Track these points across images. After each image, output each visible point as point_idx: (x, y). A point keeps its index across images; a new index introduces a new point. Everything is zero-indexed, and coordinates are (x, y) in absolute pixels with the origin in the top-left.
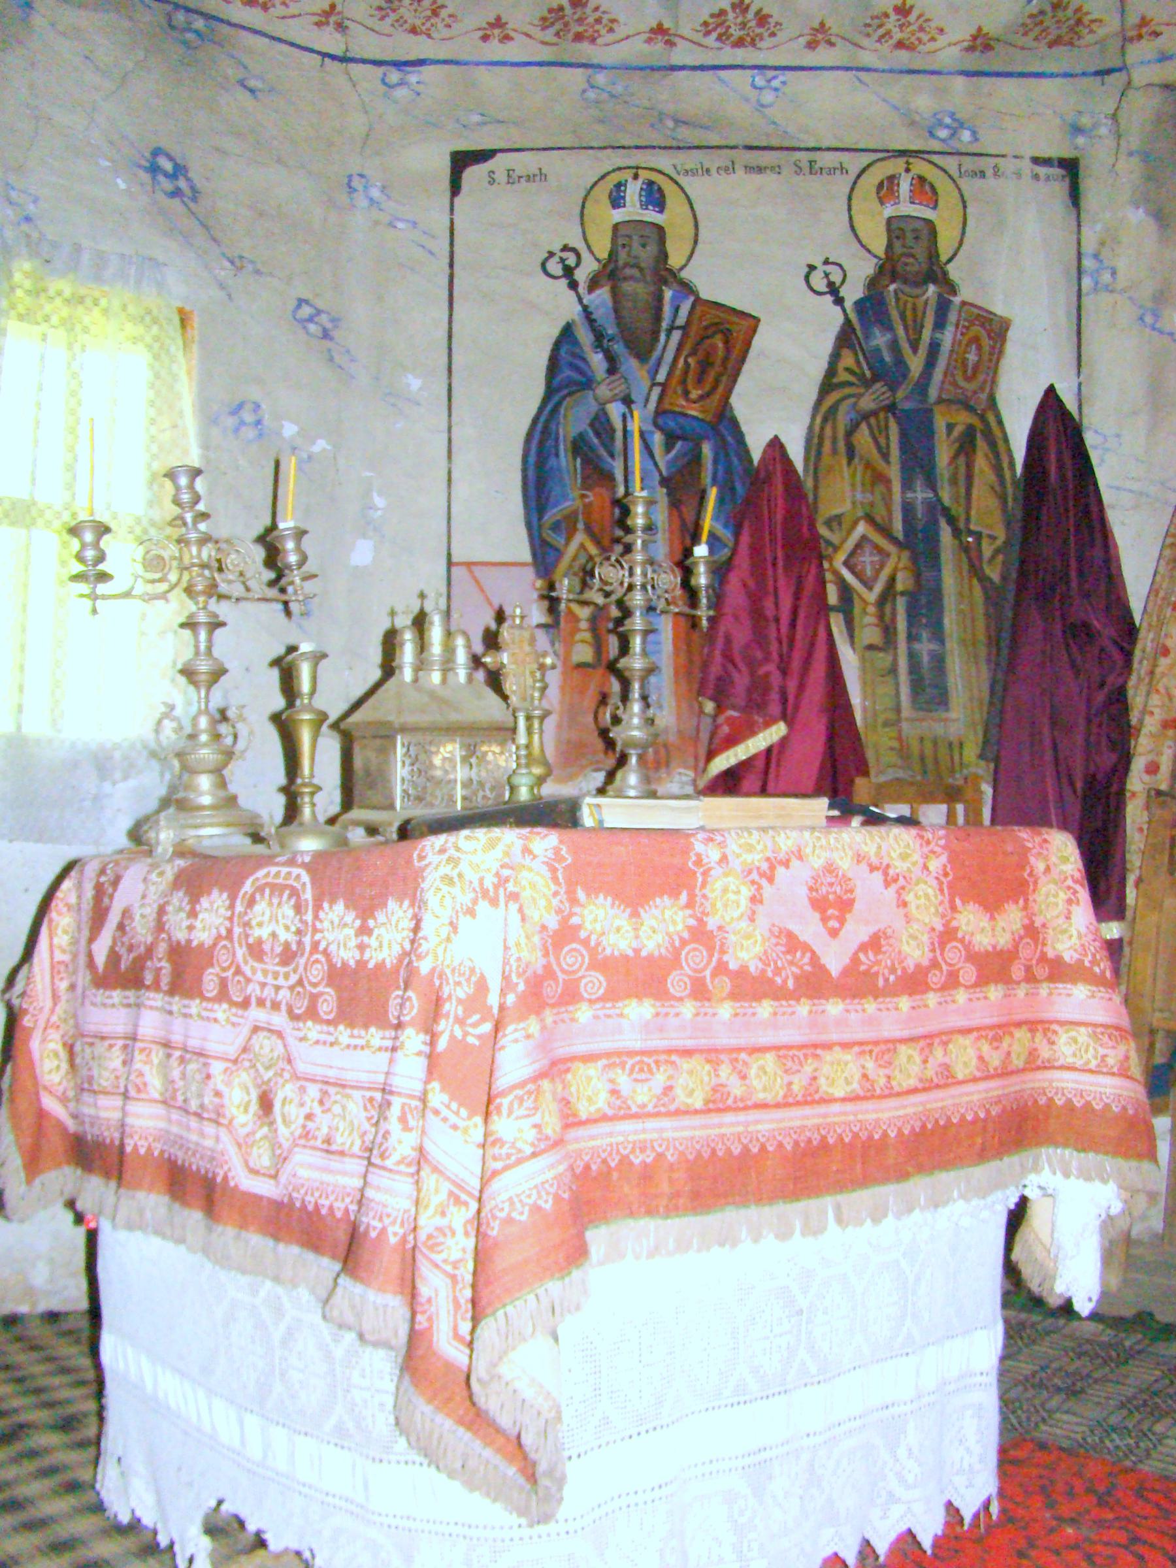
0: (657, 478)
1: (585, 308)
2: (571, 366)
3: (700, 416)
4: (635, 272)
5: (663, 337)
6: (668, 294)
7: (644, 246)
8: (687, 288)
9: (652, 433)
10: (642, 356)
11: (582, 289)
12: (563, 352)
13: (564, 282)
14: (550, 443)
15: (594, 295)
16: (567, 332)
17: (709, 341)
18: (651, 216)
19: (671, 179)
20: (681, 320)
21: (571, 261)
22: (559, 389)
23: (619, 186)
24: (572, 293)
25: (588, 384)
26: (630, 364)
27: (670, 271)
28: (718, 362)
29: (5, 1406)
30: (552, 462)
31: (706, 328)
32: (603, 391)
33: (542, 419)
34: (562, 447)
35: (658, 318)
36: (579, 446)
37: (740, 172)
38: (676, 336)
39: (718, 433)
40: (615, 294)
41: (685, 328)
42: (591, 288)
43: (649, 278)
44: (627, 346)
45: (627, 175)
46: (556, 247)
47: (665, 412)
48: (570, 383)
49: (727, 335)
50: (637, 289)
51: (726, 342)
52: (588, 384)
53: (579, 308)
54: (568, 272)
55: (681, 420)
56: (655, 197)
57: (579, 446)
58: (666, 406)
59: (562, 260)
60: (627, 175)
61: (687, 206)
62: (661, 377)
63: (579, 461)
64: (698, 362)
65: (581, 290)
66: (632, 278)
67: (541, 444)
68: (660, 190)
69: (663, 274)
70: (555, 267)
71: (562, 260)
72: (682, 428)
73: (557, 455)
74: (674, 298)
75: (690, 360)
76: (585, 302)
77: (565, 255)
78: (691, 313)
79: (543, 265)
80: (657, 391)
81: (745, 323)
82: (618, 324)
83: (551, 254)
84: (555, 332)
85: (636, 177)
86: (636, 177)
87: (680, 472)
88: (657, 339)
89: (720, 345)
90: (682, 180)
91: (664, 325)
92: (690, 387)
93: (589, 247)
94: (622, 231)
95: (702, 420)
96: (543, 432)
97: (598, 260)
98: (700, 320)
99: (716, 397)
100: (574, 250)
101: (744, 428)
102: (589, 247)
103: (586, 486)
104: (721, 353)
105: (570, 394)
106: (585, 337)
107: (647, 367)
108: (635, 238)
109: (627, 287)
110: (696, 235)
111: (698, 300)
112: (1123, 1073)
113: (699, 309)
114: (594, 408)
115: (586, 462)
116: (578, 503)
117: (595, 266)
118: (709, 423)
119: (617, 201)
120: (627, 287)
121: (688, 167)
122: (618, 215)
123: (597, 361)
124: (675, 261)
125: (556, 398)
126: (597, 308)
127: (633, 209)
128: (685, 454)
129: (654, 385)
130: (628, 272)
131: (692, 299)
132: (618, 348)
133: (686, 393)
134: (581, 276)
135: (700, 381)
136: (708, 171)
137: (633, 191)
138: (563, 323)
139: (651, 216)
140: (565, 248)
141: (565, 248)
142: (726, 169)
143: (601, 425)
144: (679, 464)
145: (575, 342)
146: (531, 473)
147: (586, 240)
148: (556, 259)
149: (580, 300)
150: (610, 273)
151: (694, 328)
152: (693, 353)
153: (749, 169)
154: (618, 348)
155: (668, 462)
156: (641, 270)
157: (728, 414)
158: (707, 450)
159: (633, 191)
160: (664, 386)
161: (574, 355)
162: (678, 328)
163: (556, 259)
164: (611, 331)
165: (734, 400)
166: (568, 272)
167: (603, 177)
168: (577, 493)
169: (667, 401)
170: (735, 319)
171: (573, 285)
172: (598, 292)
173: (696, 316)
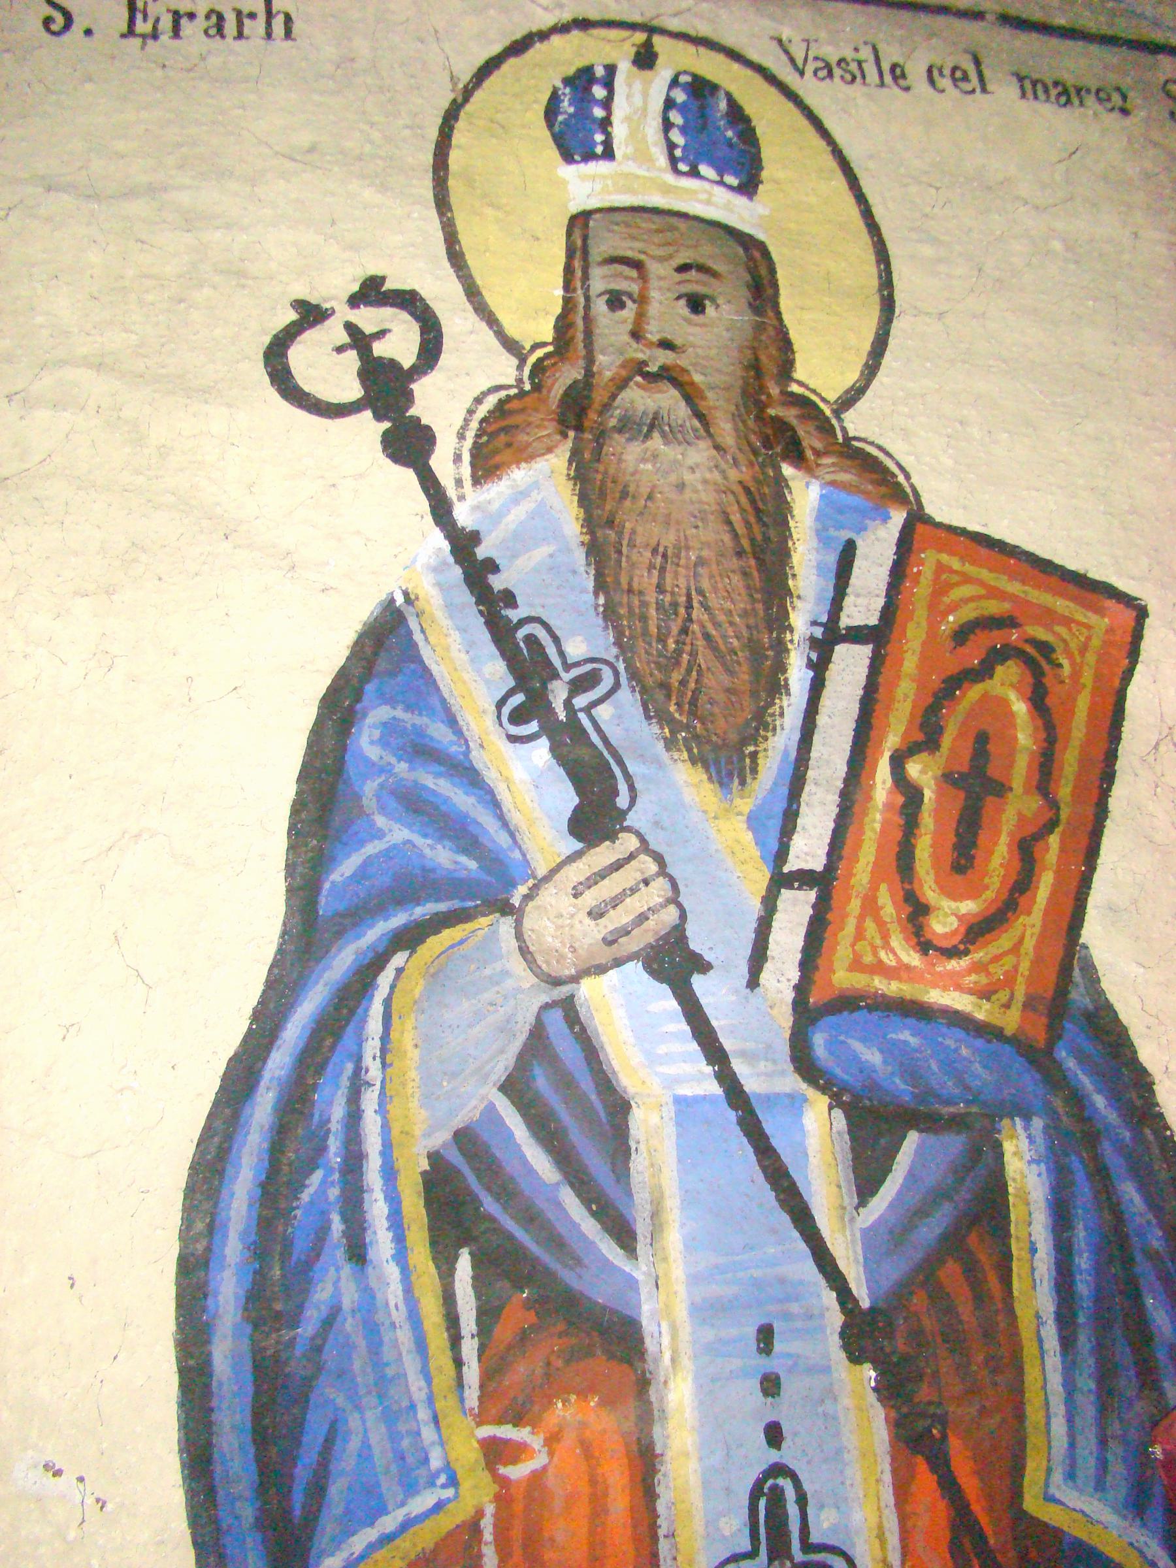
0: (836, 1319)
1: (463, 545)
2: (415, 805)
3: (982, 1012)
4: (668, 400)
5: (798, 675)
6: (806, 496)
7: (696, 304)
8: (877, 478)
9: (796, 1103)
10: (728, 762)
11: (445, 462)
12: (367, 741)
13: (368, 429)
14: (320, 1185)
15: (497, 491)
16: (386, 642)
17: (974, 692)
18: (709, 198)
19: (771, 79)
20: (861, 609)
21: (400, 343)
22: (356, 916)
23: (581, 81)
24: (408, 476)
25: (494, 890)
26: (671, 790)
27: (806, 406)
28: (1020, 772)
29: (5, 472)
30: (334, 1284)
31: (962, 635)
32: (559, 919)
33: (279, 1062)
34: (377, 1209)
35: (773, 587)
36: (458, 1200)
37: (1005, 92)
38: (851, 665)
39: (1054, 1078)
40: (596, 492)
41: (879, 636)
42: (486, 465)
43: (725, 430)
44: (653, 712)
45: (616, 50)
46: (334, 286)
47: (847, 1002)
48: (409, 885)
49: (1038, 661)
50: (682, 473)
51: (1038, 700)
52: (494, 890)
53: (438, 541)
54: (386, 389)
55: (906, 1035)
56: (711, 129)
57: (458, 1200)
58: (843, 978)
59: (359, 340)
60: (616, 50)
61: (839, 183)
62: (809, 849)
63: (464, 1265)
64: (948, 778)
65: (441, 463)
66: (655, 423)
67: (276, 1190)
68: (736, 114)
69: (781, 426)
70: (326, 367)
71: (359, 340)
72: (912, 1073)
73: (358, 1253)
74: (826, 516)
75: (913, 769)
76: (463, 516)
77: (368, 318)
78: (899, 571)
79: (276, 356)
80: (796, 908)
81: (1101, 623)
82: (610, 614)
83: (311, 315)
84: (333, 651)
85: (645, 59)
86: (645, 59)
87: (925, 1275)
88: (776, 687)
89: (1020, 707)
90: (811, 90)
91: (802, 620)
92: (930, 893)
93: (473, 293)
94: (605, 243)
95: (980, 1030)
96: (281, 1132)
97: (511, 345)
98: (937, 611)
99: (1030, 924)
100: (408, 301)
101: (1148, 1054)
102: (473, 293)
103: (505, 1401)
104: (1025, 738)
105: (409, 938)
106: (468, 672)
107: (745, 805)
108: (655, 269)
109: (631, 457)
110: (886, 283)
111: (917, 518)
112: (708, 449)
113: (927, 561)
114: (526, 999)
115: (502, 1265)
116: (476, 1494)
117: (505, 371)
118: (1020, 1044)
119: (577, 125)
120: (631, 457)
121: (832, 54)
122: (585, 186)
123: (529, 784)
124: (821, 369)
125: (342, 961)
126: (521, 541)
127: (638, 167)
128: (939, 1195)
129: (781, 881)
130: (639, 399)
131: (898, 517)
132: (619, 718)
133: (917, 912)
134: (441, 408)
135: (963, 858)
136: (898, 73)
137: (637, 107)
138: (360, 612)
139: (709, 198)
140: (371, 292)
141: (371, 292)
142: (958, 76)
143: (565, 1086)
144: (930, 1230)
145: (422, 688)
146: (226, 1353)
147: (456, 257)
148: (333, 332)
149: (441, 509)
150: (564, 404)
151: (913, 636)
152: (926, 737)
153: (1031, 86)
154: (619, 718)
155: (868, 1235)
156: (690, 394)
157: (1078, 996)
158: (1022, 1160)
159: (637, 107)
160: (823, 882)
161: (421, 751)
162: (857, 635)
163: (333, 332)
164: (582, 641)
165: (1097, 935)
166: (386, 389)
167: (518, 48)
168: (464, 1443)
169: (841, 950)
170: (1061, 605)
171: (409, 444)
172: (519, 475)
173: (920, 591)
